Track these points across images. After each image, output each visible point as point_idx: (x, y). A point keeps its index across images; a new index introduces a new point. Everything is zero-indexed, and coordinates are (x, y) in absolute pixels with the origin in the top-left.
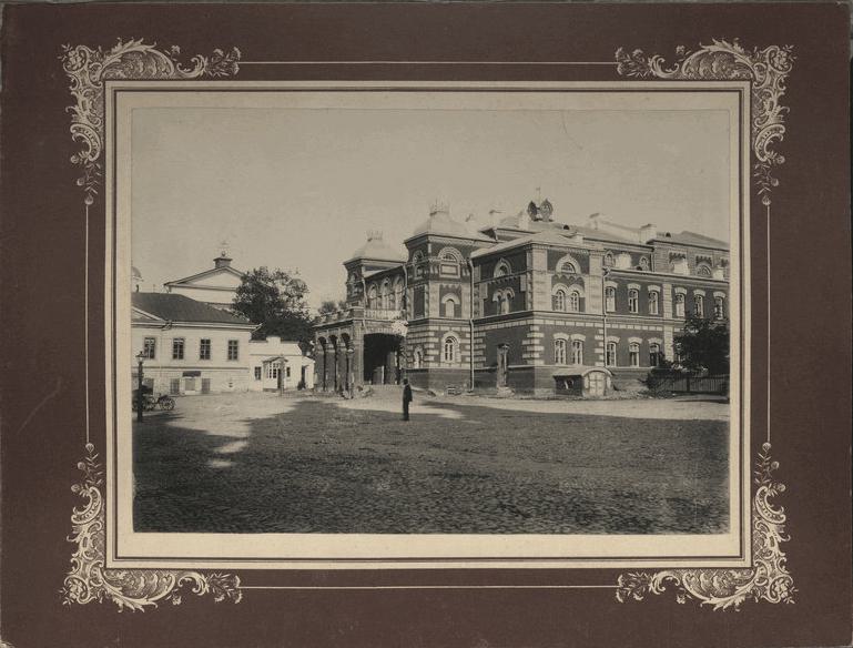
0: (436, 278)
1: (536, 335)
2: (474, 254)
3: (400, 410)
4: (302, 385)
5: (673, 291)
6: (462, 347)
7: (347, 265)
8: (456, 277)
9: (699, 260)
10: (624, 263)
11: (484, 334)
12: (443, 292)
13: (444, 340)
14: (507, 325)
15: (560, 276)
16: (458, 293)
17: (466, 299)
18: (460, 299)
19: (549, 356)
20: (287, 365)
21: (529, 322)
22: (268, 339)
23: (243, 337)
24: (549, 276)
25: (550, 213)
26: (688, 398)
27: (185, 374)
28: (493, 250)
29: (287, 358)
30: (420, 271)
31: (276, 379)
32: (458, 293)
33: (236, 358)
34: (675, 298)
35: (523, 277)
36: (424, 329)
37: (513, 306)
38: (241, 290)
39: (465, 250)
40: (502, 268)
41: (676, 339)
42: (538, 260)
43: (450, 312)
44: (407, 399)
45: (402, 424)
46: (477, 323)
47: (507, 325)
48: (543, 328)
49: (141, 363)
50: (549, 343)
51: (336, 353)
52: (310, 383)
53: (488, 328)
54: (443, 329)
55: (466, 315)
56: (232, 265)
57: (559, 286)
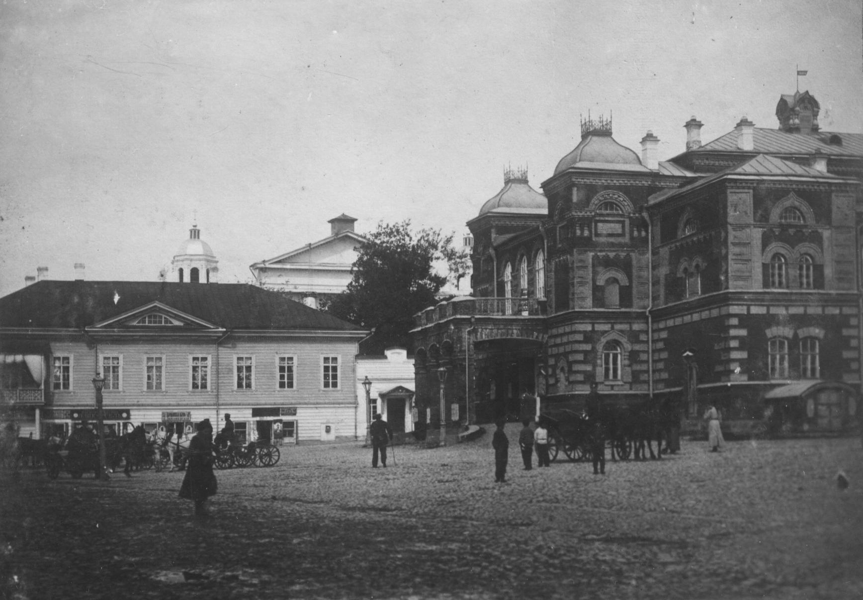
0: (587, 244)
1: (733, 332)
6: (633, 357)
11: (664, 335)
13: (600, 347)
14: (687, 319)
16: (626, 266)
18: (630, 277)
21: (724, 311)
22: (388, 353)
23: (345, 353)
25: (815, 115)
36: (568, 329)
46: (658, 315)
47: (687, 319)
48: (745, 320)
53: (670, 323)
54: (600, 327)
55: (642, 304)
57: (775, 247)
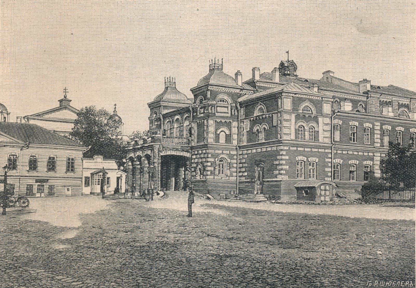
2: (240, 100)
3: (185, 208)
4: (117, 191)
5: (381, 128)
7: (150, 105)
8: (227, 115)
9: (400, 106)
10: (347, 107)
12: (218, 125)
15: (301, 115)
16: (229, 125)
17: (235, 130)
18: (230, 130)
19: (292, 174)
20: (108, 176)
21: (279, 148)
24: (293, 116)
26: (389, 204)
27: (37, 181)
28: (254, 96)
29: (107, 171)
30: (202, 111)
31: (99, 186)
32: (229, 125)
33: (72, 170)
34: (383, 133)
35: (275, 116)
37: (268, 136)
38: (76, 122)
39: (234, 97)
40: (261, 109)
41: (382, 162)
42: (287, 104)
43: (222, 139)
44: (191, 202)
45: (187, 219)
49: (6, 173)
50: (293, 163)
51: (141, 168)
52: (123, 187)
56: (71, 104)
